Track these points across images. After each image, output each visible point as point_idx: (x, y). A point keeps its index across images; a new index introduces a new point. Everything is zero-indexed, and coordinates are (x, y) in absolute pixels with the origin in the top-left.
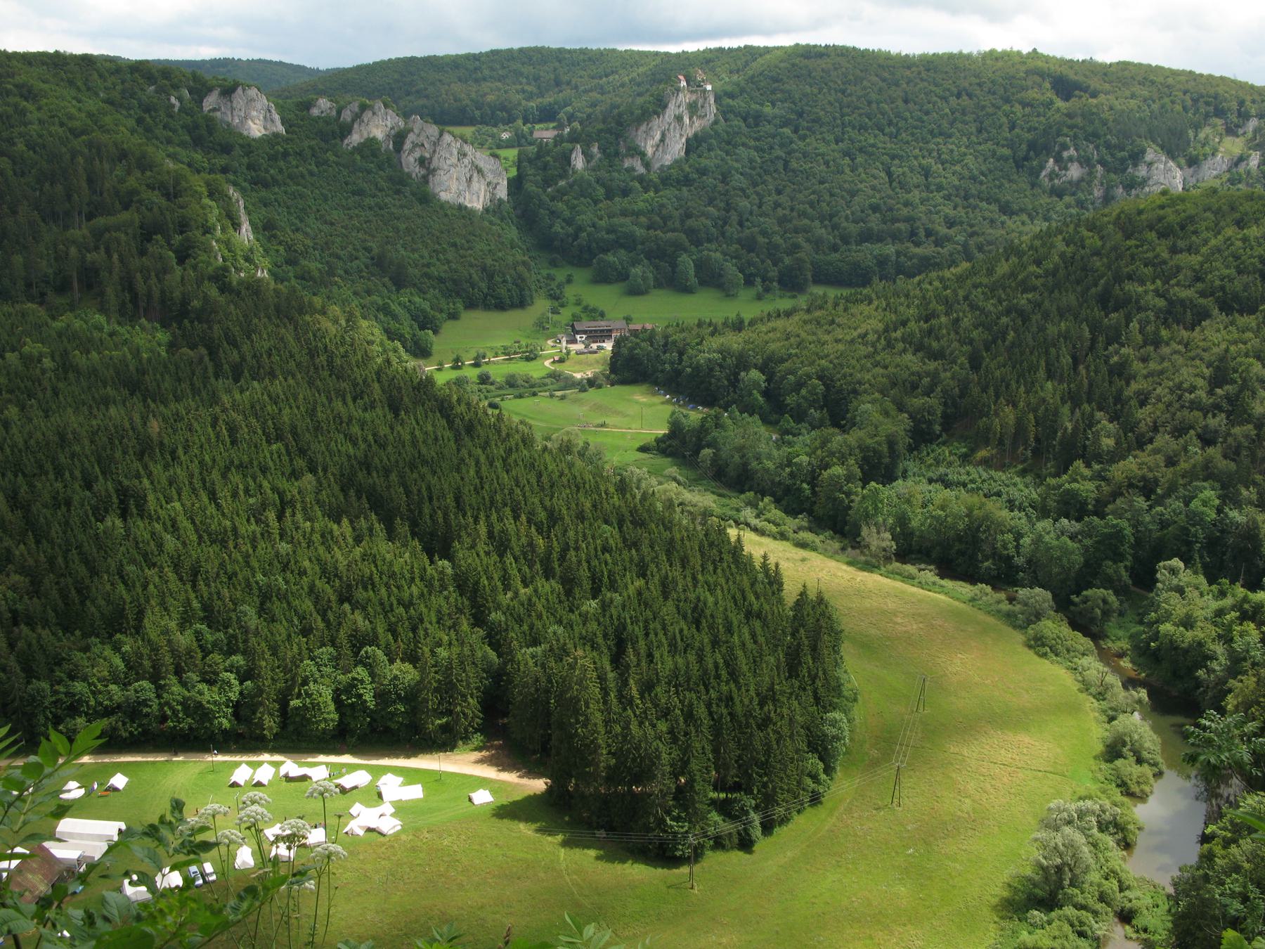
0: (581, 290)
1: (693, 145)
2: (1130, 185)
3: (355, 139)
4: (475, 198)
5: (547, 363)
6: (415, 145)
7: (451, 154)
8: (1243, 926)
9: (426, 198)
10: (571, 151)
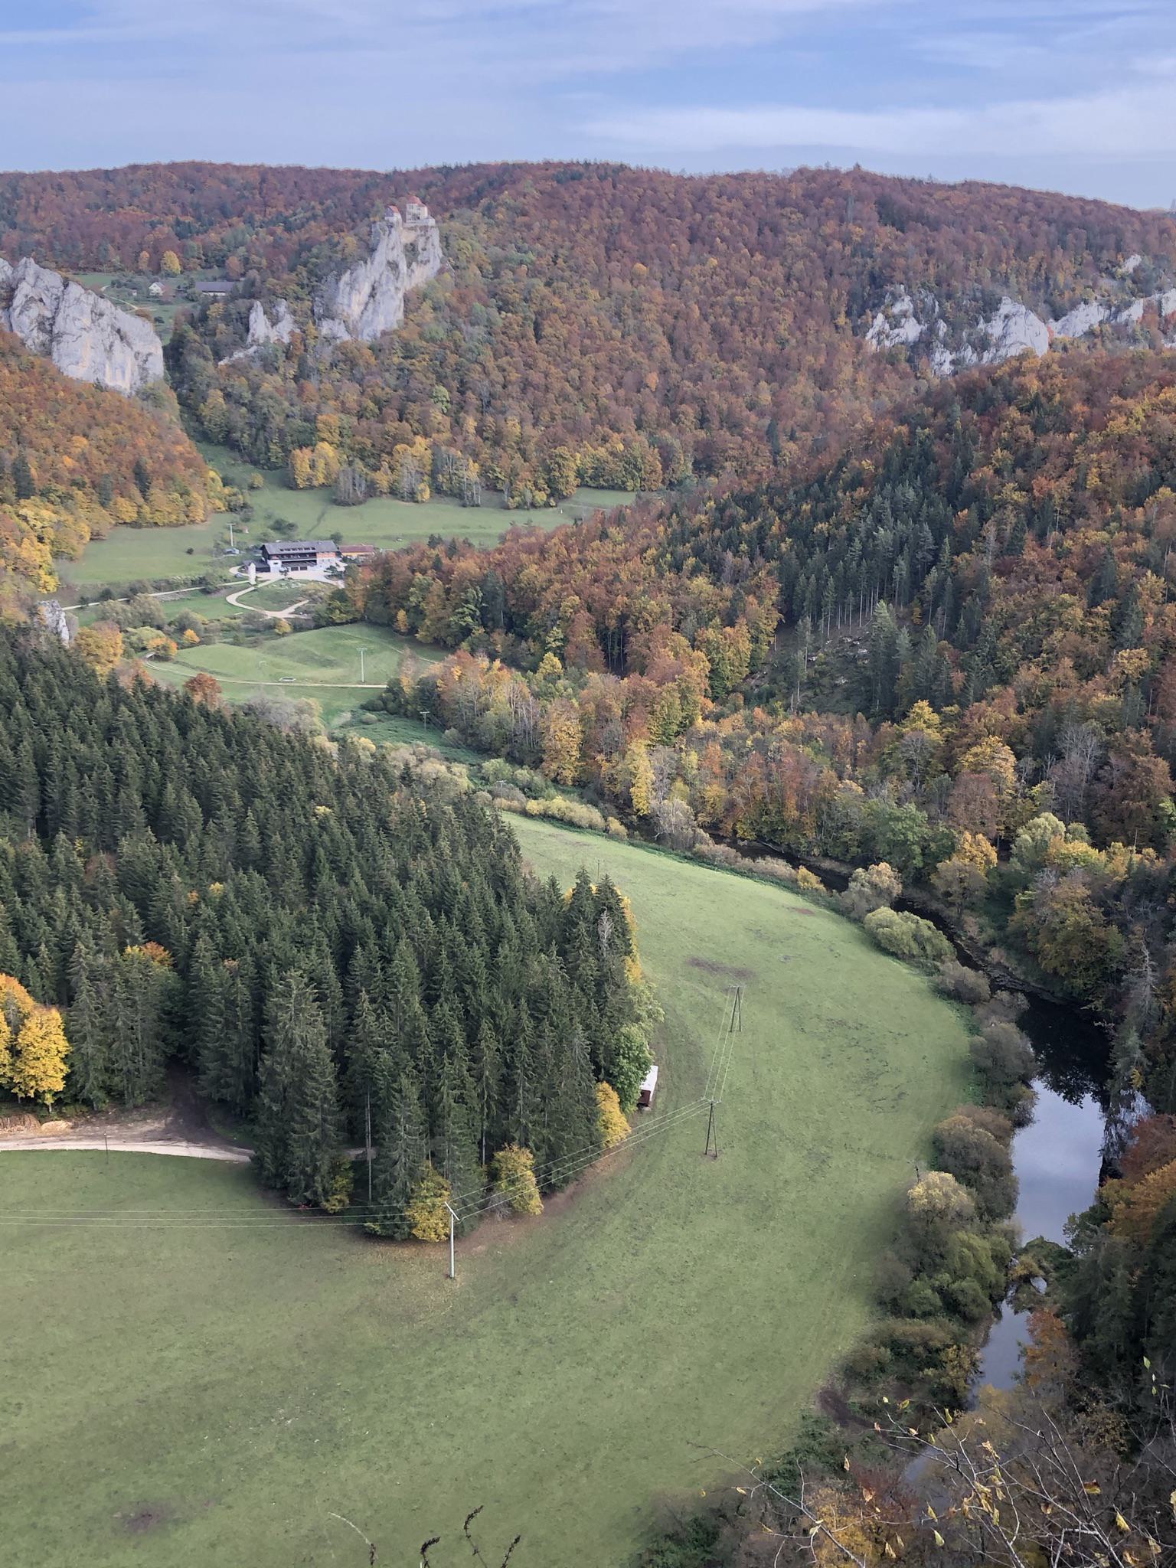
2: (982, 344)
4: (119, 372)
5: (232, 599)
6: (30, 300)
7: (82, 313)
8: (949, 410)
9: (56, 376)
10: (250, 309)
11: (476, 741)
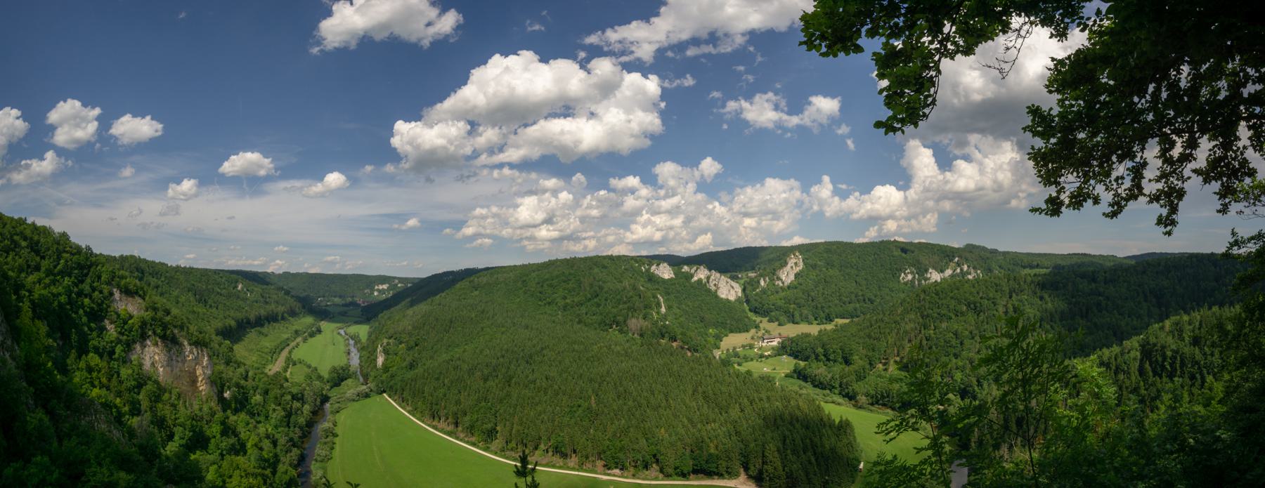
0: (765, 323)
1: (797, 275)
2: (926, 279)
3: (695, 278)
9: (717, 297)
11: (819, 385)
